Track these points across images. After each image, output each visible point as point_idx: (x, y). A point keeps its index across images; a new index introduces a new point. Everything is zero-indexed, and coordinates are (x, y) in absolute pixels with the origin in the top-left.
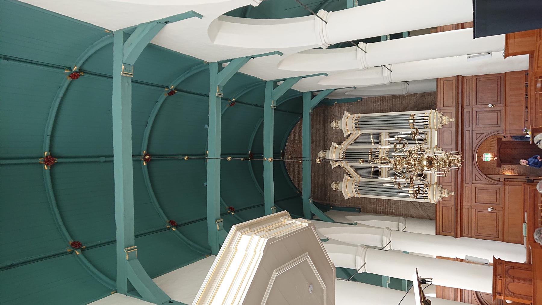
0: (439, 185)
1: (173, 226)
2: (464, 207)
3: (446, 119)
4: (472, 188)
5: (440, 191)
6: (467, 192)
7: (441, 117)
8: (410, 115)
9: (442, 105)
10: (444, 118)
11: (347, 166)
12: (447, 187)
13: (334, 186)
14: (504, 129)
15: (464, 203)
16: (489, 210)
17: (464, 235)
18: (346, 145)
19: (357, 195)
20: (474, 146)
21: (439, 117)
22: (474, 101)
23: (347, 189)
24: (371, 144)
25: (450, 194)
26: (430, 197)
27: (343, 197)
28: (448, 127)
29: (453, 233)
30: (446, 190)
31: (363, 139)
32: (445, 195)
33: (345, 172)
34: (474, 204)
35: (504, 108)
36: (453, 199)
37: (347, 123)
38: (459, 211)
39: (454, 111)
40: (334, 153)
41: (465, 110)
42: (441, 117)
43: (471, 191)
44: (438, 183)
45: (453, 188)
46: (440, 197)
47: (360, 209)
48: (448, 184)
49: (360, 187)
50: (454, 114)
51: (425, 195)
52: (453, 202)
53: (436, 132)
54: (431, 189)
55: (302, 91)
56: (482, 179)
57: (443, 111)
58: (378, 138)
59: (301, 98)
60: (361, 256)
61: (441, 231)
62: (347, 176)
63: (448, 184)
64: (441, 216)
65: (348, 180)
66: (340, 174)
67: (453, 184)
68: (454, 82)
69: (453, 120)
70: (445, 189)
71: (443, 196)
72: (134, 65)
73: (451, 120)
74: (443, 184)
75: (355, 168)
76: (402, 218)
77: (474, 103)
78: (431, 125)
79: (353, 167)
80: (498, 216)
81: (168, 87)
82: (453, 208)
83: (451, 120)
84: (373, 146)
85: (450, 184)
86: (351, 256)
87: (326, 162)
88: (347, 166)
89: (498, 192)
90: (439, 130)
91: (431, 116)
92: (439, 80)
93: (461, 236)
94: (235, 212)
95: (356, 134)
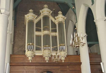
2: (24, 67)
4: (34, 69)
5: (32, 56)
6: (31, 68)
7: (49, 56)
11: (41, 17)
13: (31, 10)
15: (26, 66)
17: (11, 66)
18: (51, 18)
19: (27, 21)
21: (62, 56)
22: (71, 69)
23: (29, 16)
24: (51, 28)
26: (29, 52)
30: (32, 59)
31: (54, 25)
32: (30, 58)
34: (26, 70)
36: (28, 62)
37: (60, 18)
38: (22, 64)
39: (67, 62)
40: (46, 11)
41: (67, 66)
44: (35, 56)
45: (33, 62)
47: (16, 26)
49: (31, 23)
50: (65, 62)
52: (26, 62)
53: (42, 55)
54: (49, 51)
58: (55, 31)
60: (5, 12)
62: (36, 17)
64: (19, 57)
66: (37, 13)
67: (35, 62)
70: (32, 58)
73: (63, 61)
75: (40, 21)
76: (13, 43)
77: (70, 69)
79: (40, 21)
82: (23, 62)
83: (63, 61)
84: (51, 29)
85: (35, 60)
86: (4, 7)
88: (41, 17)
95: (57, 23)
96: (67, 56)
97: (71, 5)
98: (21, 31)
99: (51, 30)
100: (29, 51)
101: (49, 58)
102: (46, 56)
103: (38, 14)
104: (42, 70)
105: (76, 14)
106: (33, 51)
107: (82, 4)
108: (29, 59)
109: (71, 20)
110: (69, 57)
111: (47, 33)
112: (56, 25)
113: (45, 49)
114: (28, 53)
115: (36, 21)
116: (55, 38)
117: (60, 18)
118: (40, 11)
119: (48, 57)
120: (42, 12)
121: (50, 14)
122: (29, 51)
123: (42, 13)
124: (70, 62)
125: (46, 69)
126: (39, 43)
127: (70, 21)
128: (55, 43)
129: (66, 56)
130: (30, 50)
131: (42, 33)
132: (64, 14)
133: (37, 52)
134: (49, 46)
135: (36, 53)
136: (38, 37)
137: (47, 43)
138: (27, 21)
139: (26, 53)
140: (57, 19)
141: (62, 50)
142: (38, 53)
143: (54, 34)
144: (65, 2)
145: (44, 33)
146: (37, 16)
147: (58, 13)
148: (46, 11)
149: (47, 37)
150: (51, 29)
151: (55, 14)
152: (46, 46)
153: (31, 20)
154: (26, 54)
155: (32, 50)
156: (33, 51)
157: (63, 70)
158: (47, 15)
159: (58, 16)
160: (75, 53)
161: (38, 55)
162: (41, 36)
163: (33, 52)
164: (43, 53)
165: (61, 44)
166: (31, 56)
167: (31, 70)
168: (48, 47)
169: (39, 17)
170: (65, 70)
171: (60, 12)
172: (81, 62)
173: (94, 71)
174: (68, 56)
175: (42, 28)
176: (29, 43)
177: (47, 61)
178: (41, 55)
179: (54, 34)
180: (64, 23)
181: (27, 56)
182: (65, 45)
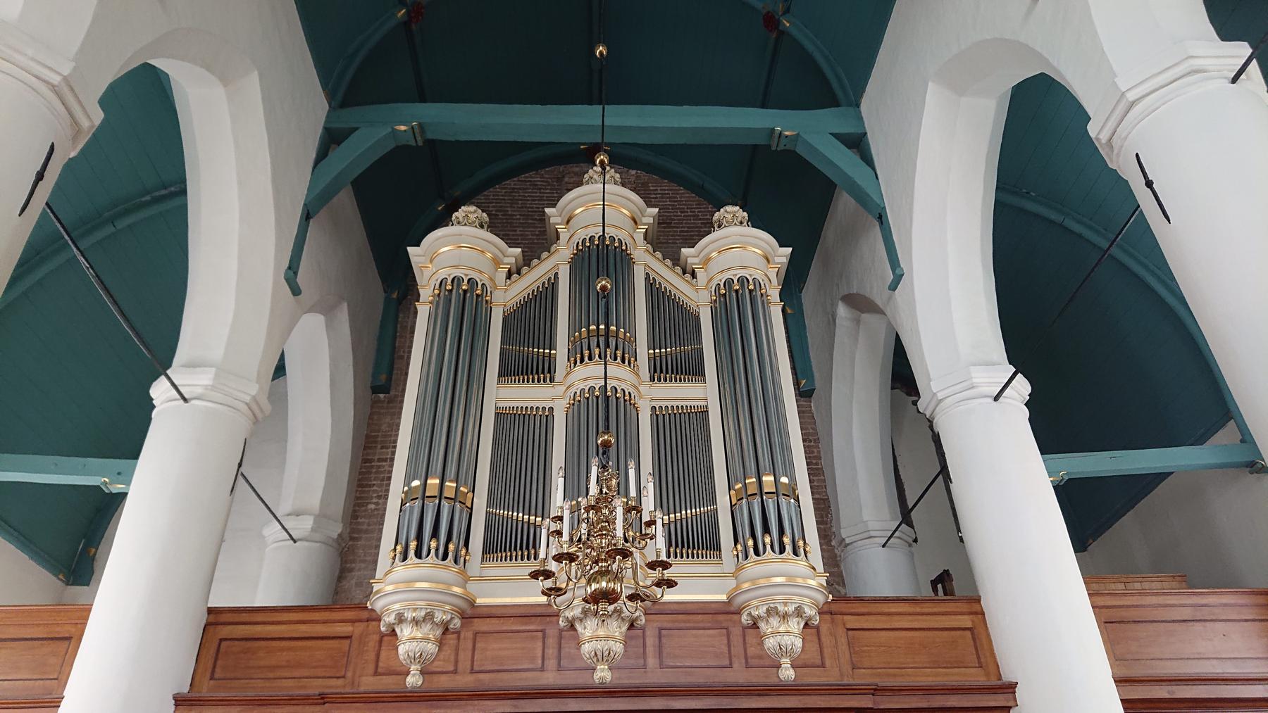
0: (464, 617)
1: (408, 13)
5: (429, 617)
7: (799, 612)
8: (792, 478)
9: (852, 622)
10: (795, 625)
11: (558, 262)
12: (448, 652)
18: (645, 262)
23: (454, 251)
24: (652, 345)
25: (415, 669)
28: (751, 651)
30: (432, 648)
31: (671, 318)
32: (413, 643)
33: (527, 260)
37: (741, 250)
42: (799, 612)
44: (471, 613)
45: (444, 682)
46: (401, 619)
48: (465, 657)
49: (465, 302)
52: (369, 683)
53: (724, 597)
57: (824, 629)
59: (830, 101)
60: (213, 388)
61: (226, 631)
63: (465, 657)
65: (497, 262)
66: (532, 238)
67: (465, 681)
68: (975, 676)
69: (787, 673)
70: (441, 643)
71: (405, 632)
72: (794, 151)
73: (786, 663)
74: (467, 635)
75: (547, 293)
78: (754, 567)
79: (547, 293)
81: (787, 11)
83: (786, 663)
85: (464, 664)
88: (558, 262)
91: (798, 566)
92: (975, 607)
94: (406, 24)
95: (698, 297)
102: (771, 612)
103: (532, 238)
105: (881, 218)
110: (852, 622)
115: (507, 296)
119: (416, 622)
123: (561, 229)
124: (864, 678)
129: (810, 612)
148: (600, 207)
153: (456, 281)
160: (927, 591)
162: (549, 416)
163: (448, 572)
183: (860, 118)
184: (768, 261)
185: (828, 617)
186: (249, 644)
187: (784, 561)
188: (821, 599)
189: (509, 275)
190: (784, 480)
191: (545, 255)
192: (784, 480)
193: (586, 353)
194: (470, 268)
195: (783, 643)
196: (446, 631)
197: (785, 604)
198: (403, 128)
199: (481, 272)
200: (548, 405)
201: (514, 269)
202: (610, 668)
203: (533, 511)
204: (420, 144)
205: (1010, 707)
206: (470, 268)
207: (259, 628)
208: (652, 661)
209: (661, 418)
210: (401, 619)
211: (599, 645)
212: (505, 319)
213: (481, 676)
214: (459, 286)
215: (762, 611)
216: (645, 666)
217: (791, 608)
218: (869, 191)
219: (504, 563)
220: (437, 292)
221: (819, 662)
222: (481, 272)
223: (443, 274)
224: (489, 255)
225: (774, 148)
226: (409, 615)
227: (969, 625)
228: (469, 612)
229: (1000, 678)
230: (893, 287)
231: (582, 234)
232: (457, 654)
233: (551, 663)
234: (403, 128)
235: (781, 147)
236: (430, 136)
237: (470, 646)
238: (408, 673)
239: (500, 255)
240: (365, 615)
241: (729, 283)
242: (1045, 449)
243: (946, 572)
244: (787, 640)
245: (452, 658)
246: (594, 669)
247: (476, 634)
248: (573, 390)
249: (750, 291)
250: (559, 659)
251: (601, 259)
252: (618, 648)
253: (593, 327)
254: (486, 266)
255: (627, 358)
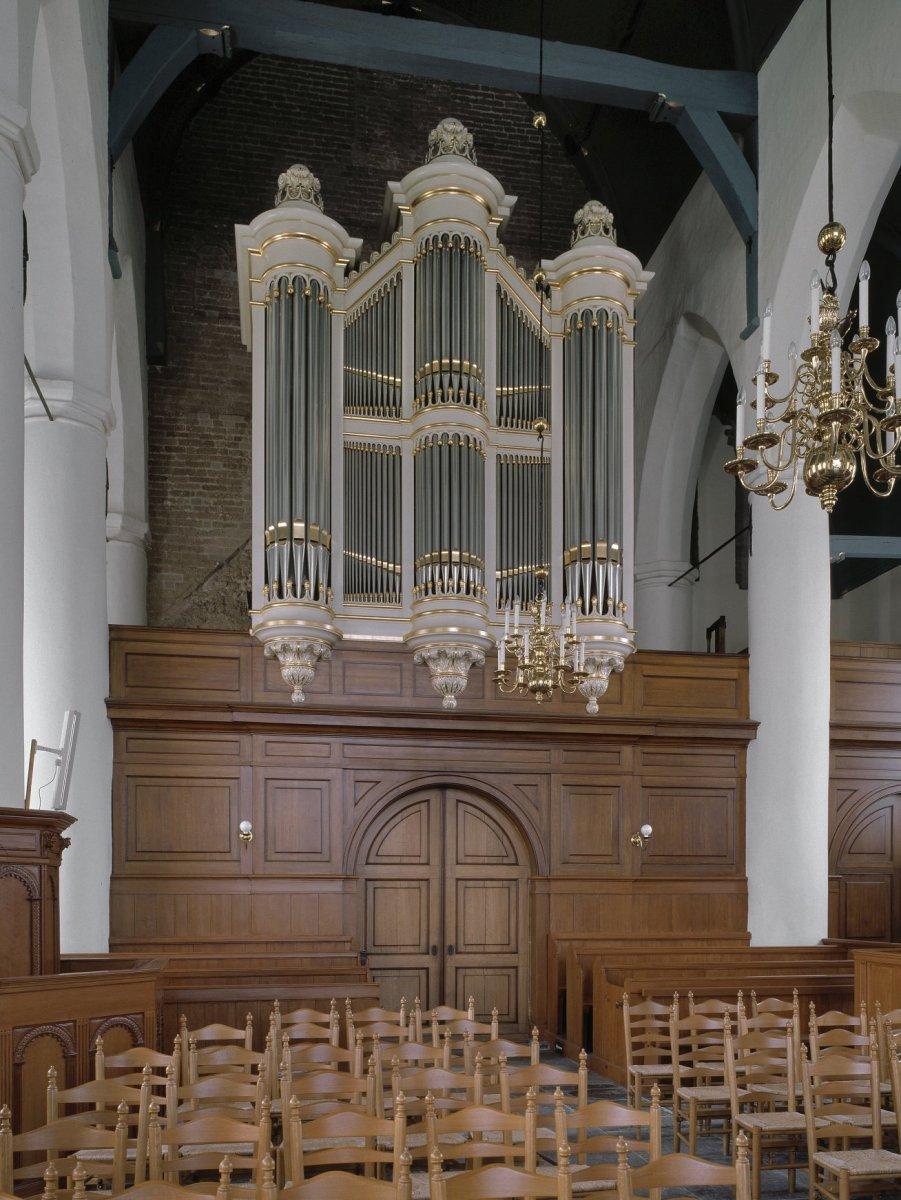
0: (331, 646)
2: (245, 739)
3: (601, 680)
4: (327, 766)
5: (310, 649)
6: (308, 750)
7: (467, 656)
9: (648, 670)
11: (401, 255)
14: (555, 874)
15: (260, 739)
16: (245, 826)
18: (498, 269)
20: (479, 776)
23: (285, 240)
26: (279, 607)
27: (238, 223)
29: (123, 694)
30: (310, 672)
31: (523, 350)
32: (291, 667)
34: (262, 773)
35: (627, 874)
37: (600, 271)
40: (453, 191)
41: (627, 751)
42: (467, 656)
43: (315, 766)
44: (337, 644)
46: (285, 649)
49: (300, 304)
51: (430, 585)
52: (261, 698)
53: (400, 639)
55: (759, 74)
56: (364, 805)
58: (523, 412)
61: (131, 647)
62: (350, 254)
65: (335, 255)
66: (372, 226)
68: (731, 715)
69: (593, 707)
70: (315, 668)
72: (674, 127)
73: (593, 700)
75: (389, 297)
79: (389, 297)
80: (218, 857)
83: (593, 700)
84: (492, 390)
87: (416, 150)
89: (317, 857)
90: (402, 651)
93: (117, 724)
95: (553, 332)
96: (630, 661)
97: (719, 143)
98: (214, 414)
99: (500, 397)
100: (280, 595)
101: (463, 669)
102: (442, 654)
103: (372, 226)
104: (403, 777)
105: (751, 243)
106: (316, 597)
107: (682, 318)
108: (286, 672)
109: (695, 321)
110: (648, 670)
111: (457, 430)
112: (543, 351)
113: (430, 589)
114: (275, 619)
115: (346, 302)
116: (524, 483)
117: (600, 271)
118: (391, 184)
119: (299, 653)
120: (415, 204)
121: (492, 229)
122: (280, 595)
123: (406, 214)
124: (650, 713)
125: (437, 766)
126: (371, 518)
127: (682, 329)
128: (524, 533)
129: (620, 663)
130: (287, 584)
131: (408, 428)
132: (639, 234)
133: (360, 608)
134: (470, 563)
135: (549, 784)
136: (371, 470)
137: (448, 528)
138: (261, 291)
139: (257, 620)
140: (556, 292)
141: (593, 600)
142: (371, 626)
143: (521, 443)
144: (656, 96)
145: (429, 431)
146: (359, 242)
147: (579, 214)
148: (453, 191)
149: (451, 463)
150: (492, 390)
151: (537, 237)
152: (505, 389)
153: (298, 281)
154: (254, 623)
155: (310, 586)
156: (316, 597)
157: (586, 780)
158: (457, 239)
159: (568, 247)
160: (700, 644)
161: (369, 638)
162: (396, 460)
163: (319, 612)
164: (408, 628)
165: (582, 542)
166: (303, 646)
167: (301, 773)
168: (460, 563)
169: (375, 255)
170: (604, 780)
171: (595, 213)
172: (754, 717)
173: (857, 796)
174: (639, 658)
175: (407, 381)
176: (283, 525)
177: (450, 702)
178: (391, 639)
179: (521, 443)
180: (628, 329)
181: (261, 645)
182: (617, 559)
183: (754, 93)
184: (628, 285)
185: (631, 665)
186: (150, 658)
187: (606, 621)
188: (628, 651)
189: (347, 273)
190: (615, 547)
191: (386, 246)
192: (615, 547)
193: (439, 392)
194: (308, 266)
195: (595, 685)
196: (320, 658)
197: (602, 657)
198: (213, 33)
199: (319, 270)
200: (395, 443)
201: (353, 264)
202: (456, 698)
203: (385, 557)
204: (229, 56)
205: (749, 740)
206: (308, 266)
207: (156, 645)
208: (489, 694)
209: (504, 467)
210: (285, 649)
211: (449, 681)
212: (346, 330)
213: (353, 697)
214: (301, 290)
215: (278, 647)
216: (483, 697)
217: (606, 660)
218: (748, 212)
219: (362, 604)
220: (276, 294)
221: (618, 700)
222: (319, 270)
223: (281, 271)
224: (325, 244)
225: (652, 118)
226: (294, 646)
227: (736, 676)
228: (338, 645)
229: (748, 718)
230: (745, 335)
231: (433, 230)
232: (330, 680)
233: (409, 692)
234: (213, 33)
235: (661, 119)
236: (241, 45)
237: (340, 672)
238: (292, 692)
239: (339, 245)
240: (247, 641)
241: (587, 314)
242: (832, 532)
243: (723, 618)
244: (598, 683)
245: (328, 682)
246: (443, 697)
247: (344, 663)
248: (425, 433)
249: (608, 329)
250: (415, 687)
251: (450, 260)
252: (464, 683)
253: (446, 361)
254: (324, 261)
255: (473, 401)
